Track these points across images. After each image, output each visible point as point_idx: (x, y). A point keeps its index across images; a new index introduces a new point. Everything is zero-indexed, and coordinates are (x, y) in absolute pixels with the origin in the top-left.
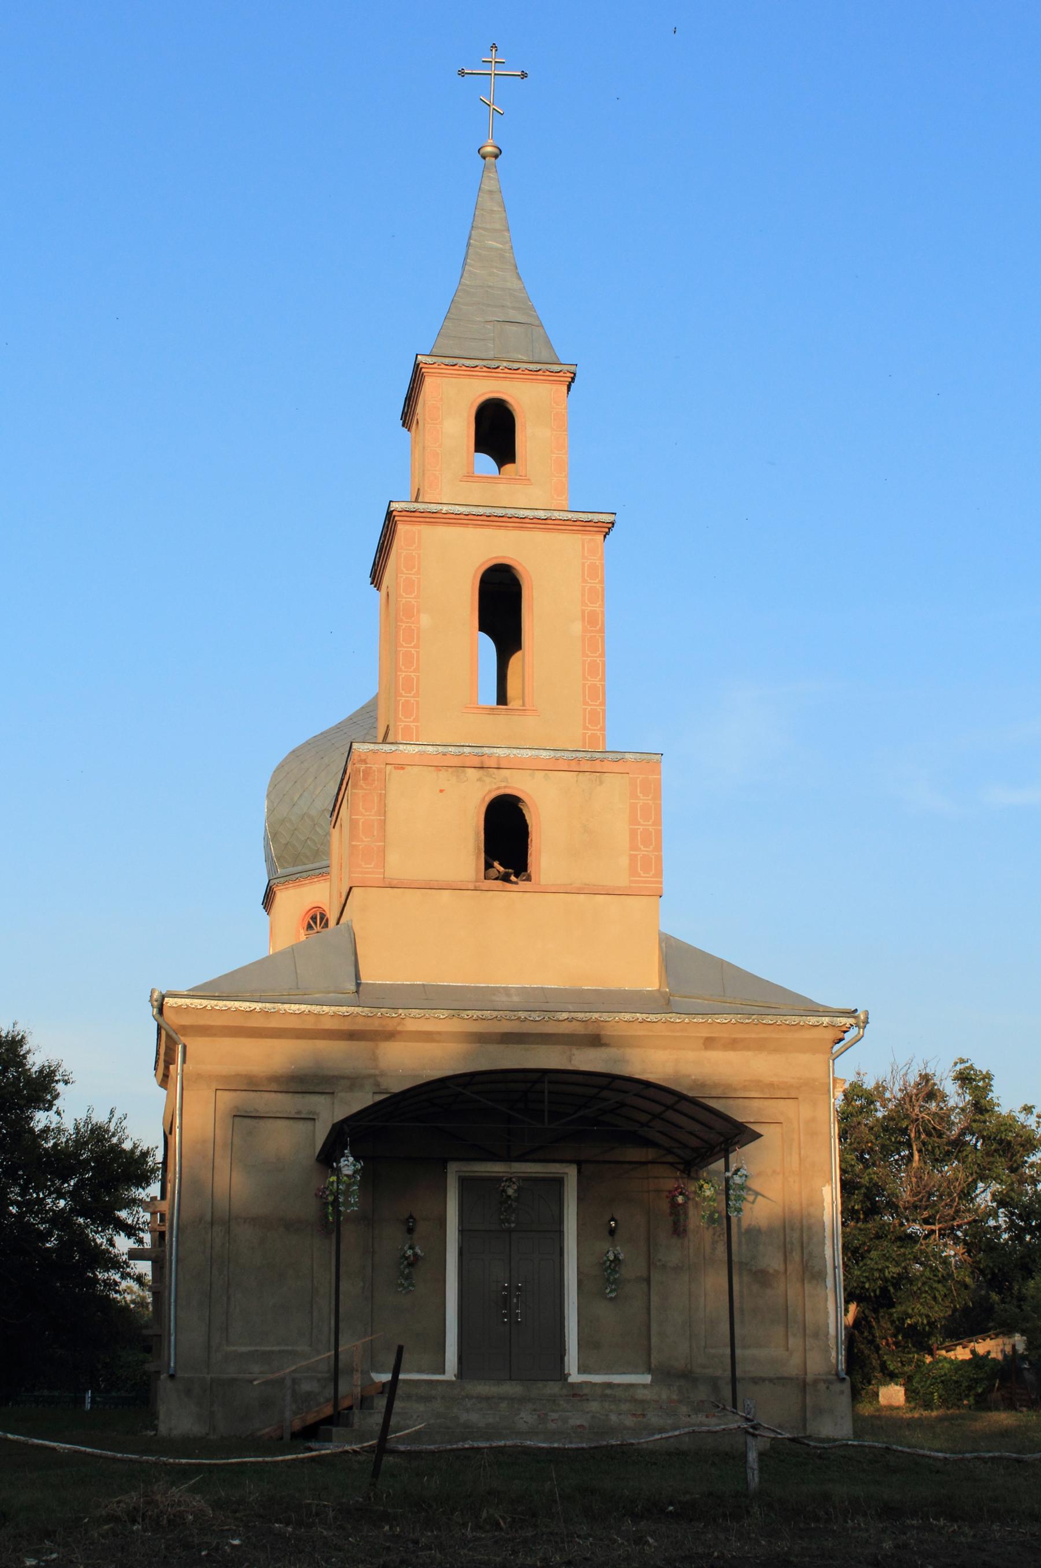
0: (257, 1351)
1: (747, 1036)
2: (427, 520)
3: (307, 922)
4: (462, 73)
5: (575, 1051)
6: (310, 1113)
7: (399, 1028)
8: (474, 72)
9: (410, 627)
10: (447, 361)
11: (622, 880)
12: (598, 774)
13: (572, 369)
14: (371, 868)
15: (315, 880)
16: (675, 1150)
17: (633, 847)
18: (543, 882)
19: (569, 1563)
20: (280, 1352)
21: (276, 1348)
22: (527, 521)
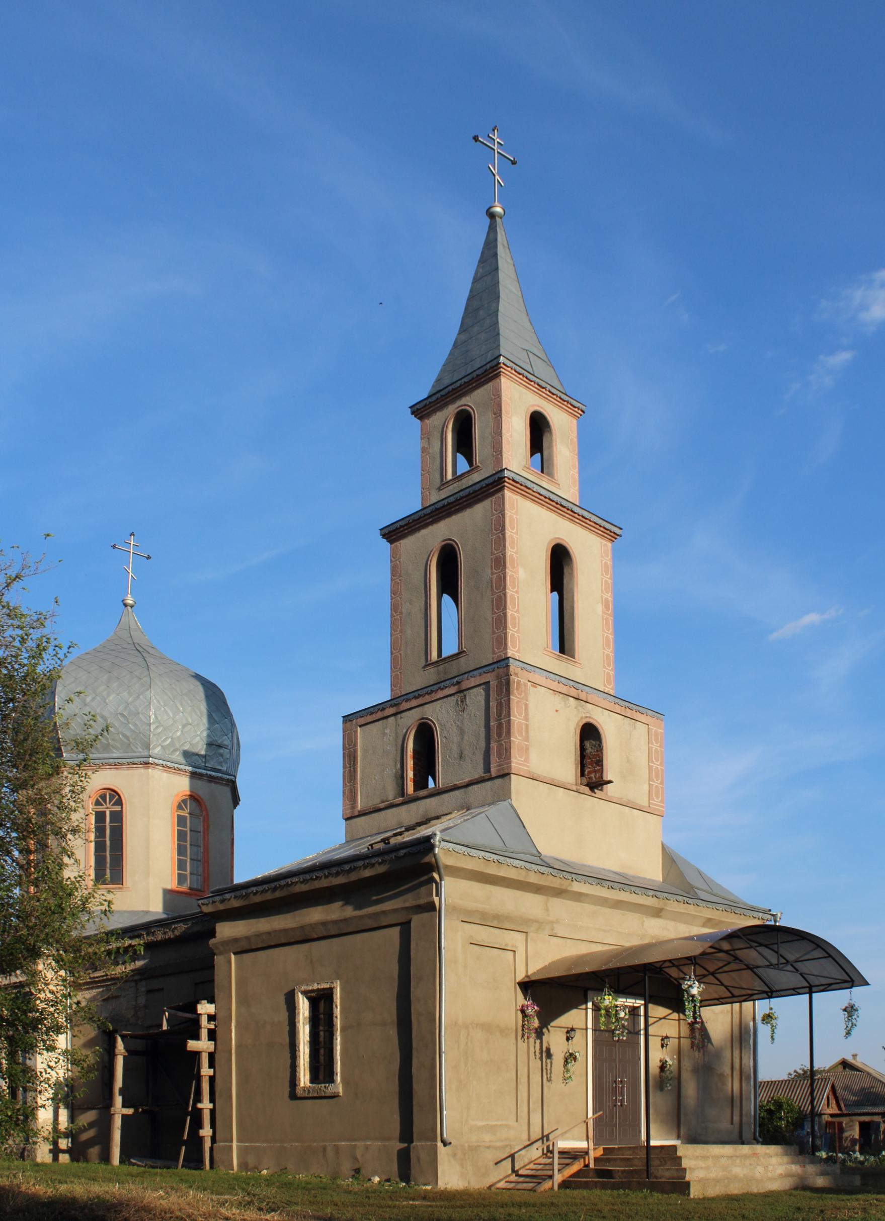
0: (487, 1125)
1: (726, 920)
2: (523, 493)
3: (95, 799)
4: (476, 139)
5: (645, 919)
6: (513, 946)
7: (569, 889)
8: (485, 142)
9: (513, 575)
10: (518, 369)
11: (644, 802)
12: (634, 721)
13: (584, 408)
14: (521, 761)
15: (107, 767)
16: (747, 997)
17: (650, 779)
18: (609, 794)
19: (244, 1220)
20: (501, 1125)
21: (499, 1123)
22: (576, 516)
